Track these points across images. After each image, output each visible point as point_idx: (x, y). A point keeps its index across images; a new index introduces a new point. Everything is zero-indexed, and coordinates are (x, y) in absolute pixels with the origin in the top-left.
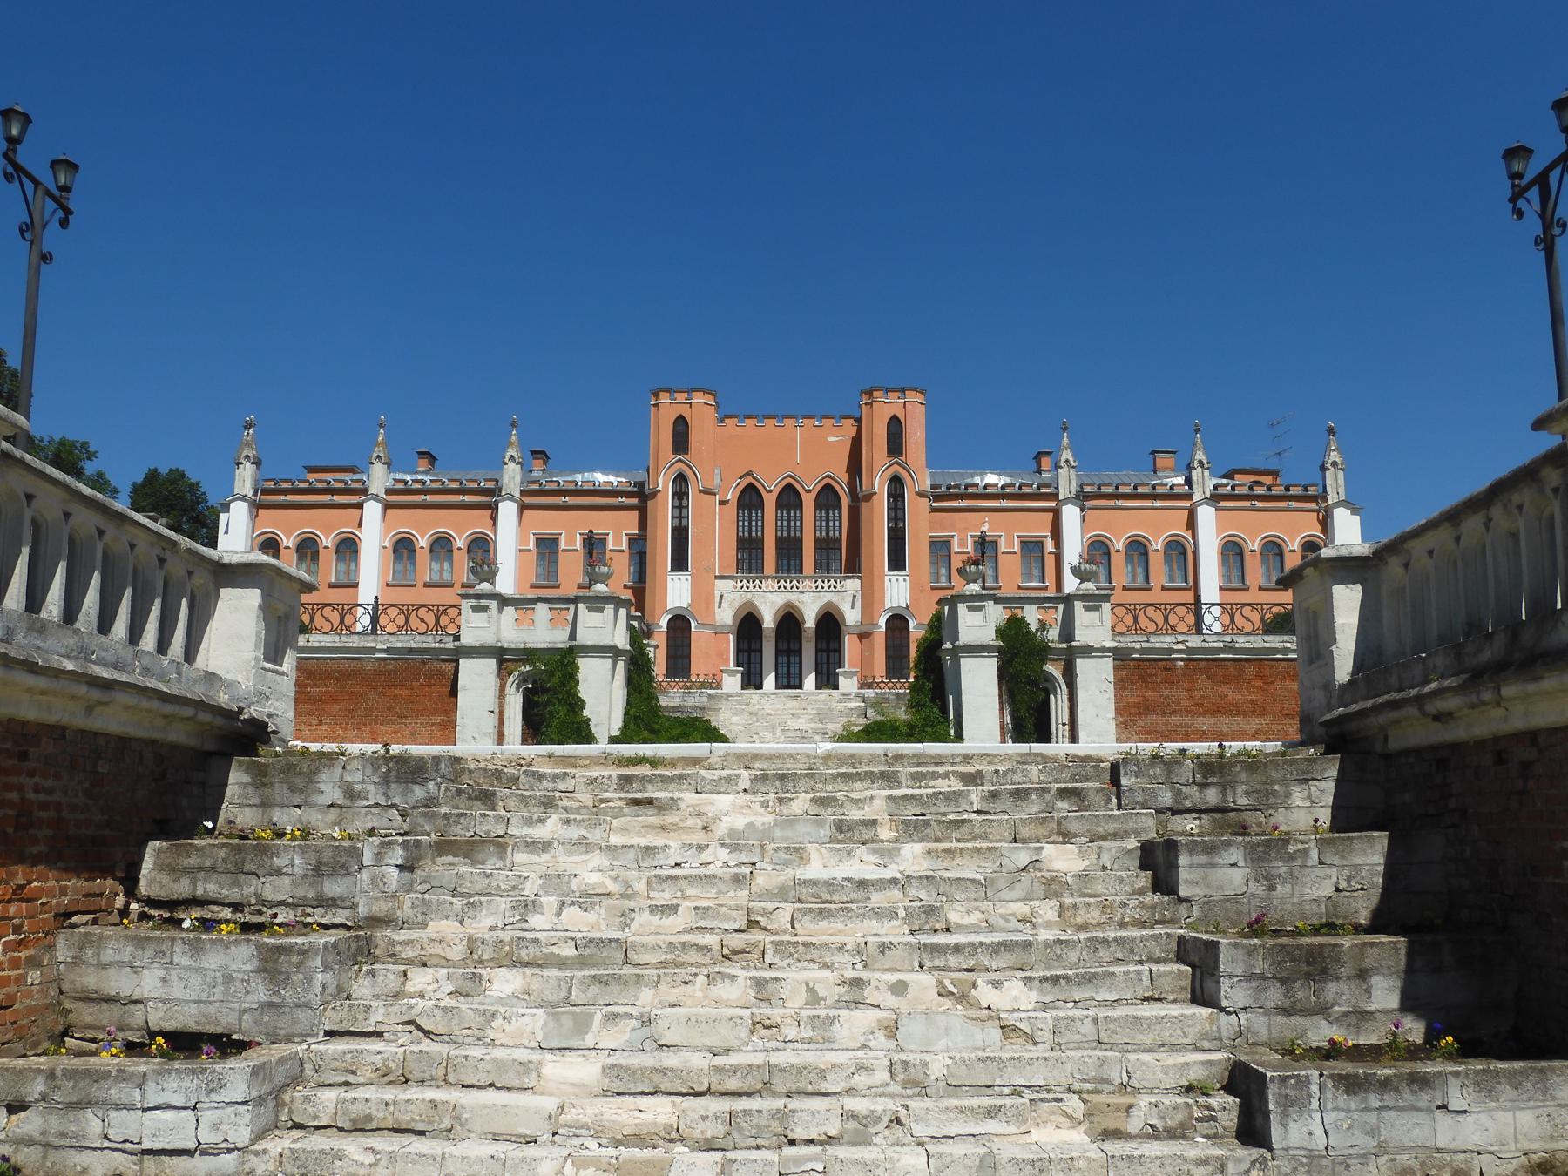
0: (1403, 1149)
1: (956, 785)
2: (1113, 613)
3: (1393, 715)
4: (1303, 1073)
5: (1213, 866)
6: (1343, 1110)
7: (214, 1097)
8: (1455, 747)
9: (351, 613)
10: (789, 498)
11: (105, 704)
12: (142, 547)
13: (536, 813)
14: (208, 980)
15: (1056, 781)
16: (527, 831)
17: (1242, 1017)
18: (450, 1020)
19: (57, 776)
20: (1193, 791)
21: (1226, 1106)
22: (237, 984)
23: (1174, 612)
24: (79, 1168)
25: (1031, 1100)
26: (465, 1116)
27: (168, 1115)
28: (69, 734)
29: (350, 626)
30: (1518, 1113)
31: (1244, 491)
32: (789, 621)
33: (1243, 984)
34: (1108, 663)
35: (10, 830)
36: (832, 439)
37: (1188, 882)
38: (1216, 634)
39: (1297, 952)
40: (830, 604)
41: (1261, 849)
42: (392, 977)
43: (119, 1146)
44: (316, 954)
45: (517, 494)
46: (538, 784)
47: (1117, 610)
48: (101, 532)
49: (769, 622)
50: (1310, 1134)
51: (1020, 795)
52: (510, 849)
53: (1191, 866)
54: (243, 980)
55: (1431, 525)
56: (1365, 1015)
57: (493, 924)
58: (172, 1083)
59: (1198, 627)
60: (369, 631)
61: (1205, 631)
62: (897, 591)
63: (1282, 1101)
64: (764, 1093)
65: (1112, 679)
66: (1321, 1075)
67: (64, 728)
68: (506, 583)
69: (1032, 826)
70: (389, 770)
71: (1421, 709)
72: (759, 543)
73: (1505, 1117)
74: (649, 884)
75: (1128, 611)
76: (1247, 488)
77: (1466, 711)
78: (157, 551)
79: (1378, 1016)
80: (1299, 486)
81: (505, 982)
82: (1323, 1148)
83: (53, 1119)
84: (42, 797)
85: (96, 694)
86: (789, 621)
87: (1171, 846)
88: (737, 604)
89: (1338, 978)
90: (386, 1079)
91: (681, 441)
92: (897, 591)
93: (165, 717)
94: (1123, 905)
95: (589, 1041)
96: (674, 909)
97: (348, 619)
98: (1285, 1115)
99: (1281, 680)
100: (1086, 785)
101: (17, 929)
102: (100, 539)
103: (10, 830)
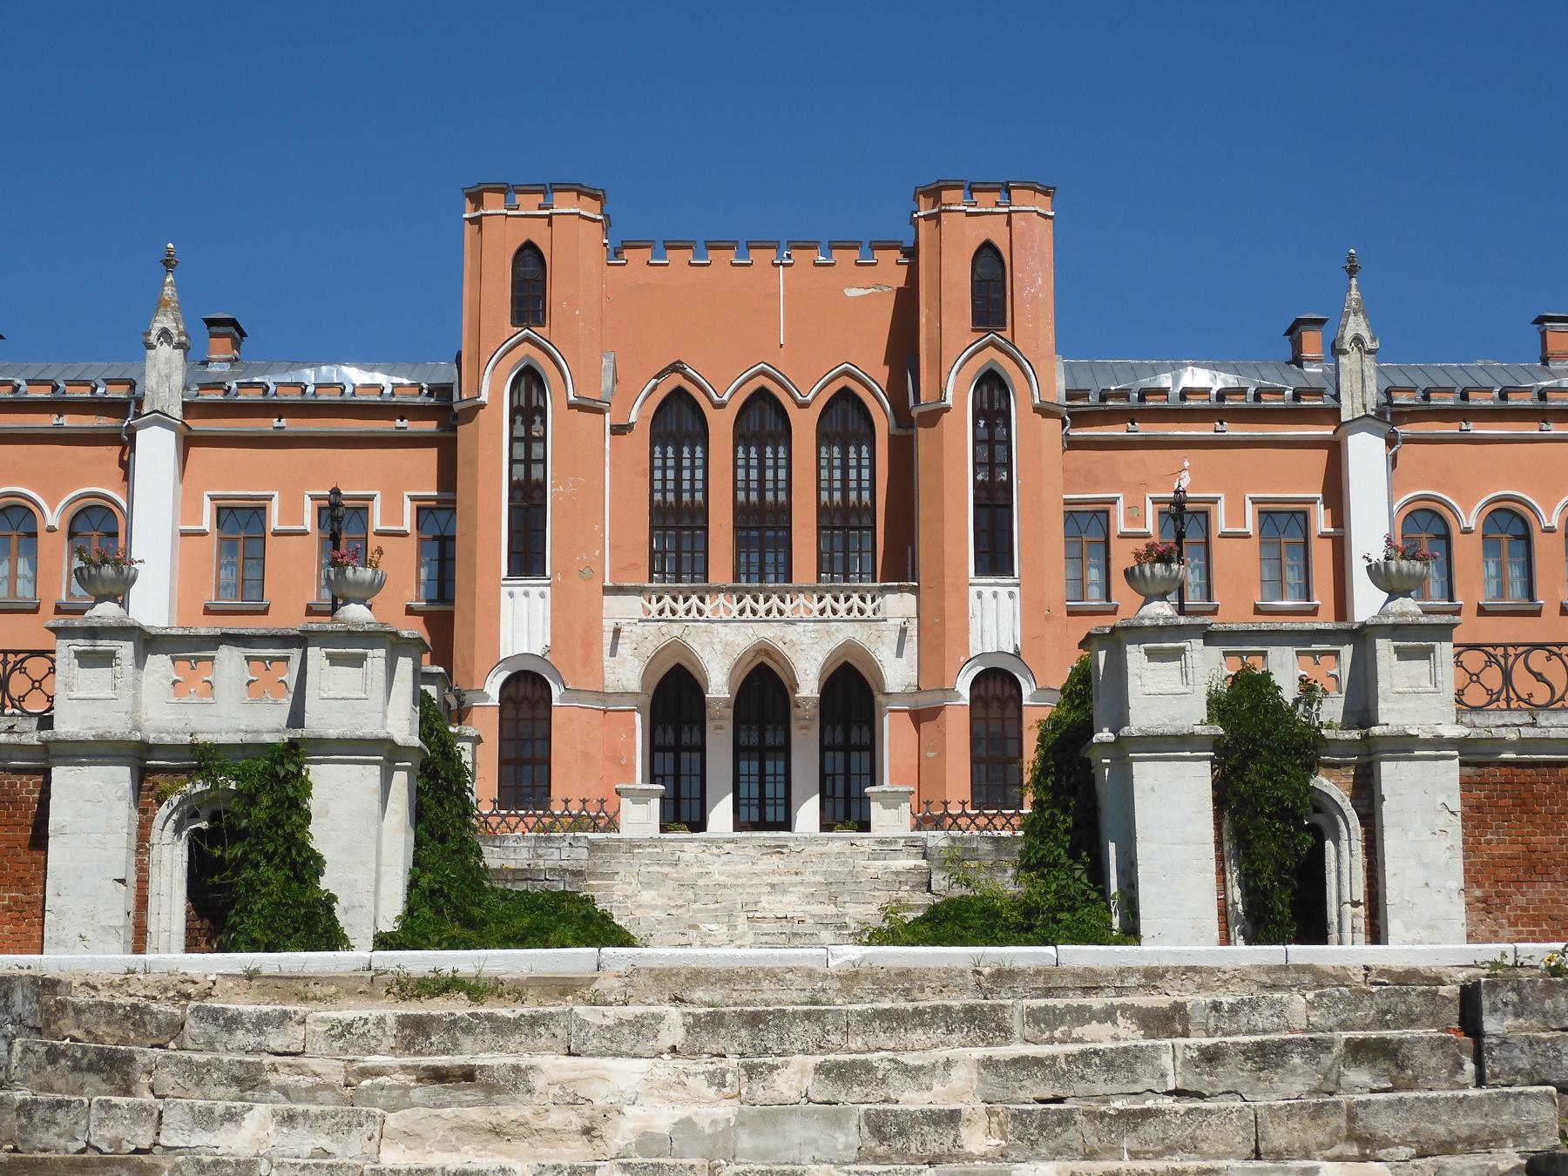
1: (1129, 1035)
2: (1459, 664)
13: (222, 1099)
15: (1343, 1026)
16: (200, 1139)
40: (850, 646)
49: (719, 685)
65: (1456, 805)
69: (1294, 1123)
75: (1491, 660)
88: (650, 649)
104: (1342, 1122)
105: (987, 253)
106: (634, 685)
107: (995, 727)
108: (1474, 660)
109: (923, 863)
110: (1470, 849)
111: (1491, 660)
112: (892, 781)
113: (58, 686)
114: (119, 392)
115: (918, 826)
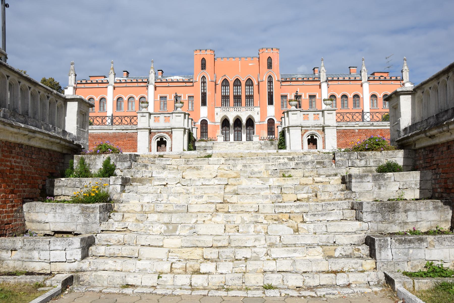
0: (415, 260)
1: (286, 160)
2: (336, 115)
3: (417, 137)
4: (386, 238)
5: (362, 182)
6: (397, 248)
7: (70, 247)
8: (435, 146)
9: (105, 119)
10: (237, 83)
11: (34, 137)
12: (42, 92)
13: (161, 170)
14: (67, 216)
15: (316, 159)
16: (158, 175)
17: (369, 224)
18: (137, 228)
19: (21, 159)
20: (358, 161)
21: (365, 250)
22: (75, 217)
23: (355, 115)
24: (33, 267)
25: (306, 248)
26: (142, 253)
27: (58, 252)
28: (24, 147)
29: (105, 123)
30: (450, 249)
31: (377, 78)
32: (238, 122)
33: (370, 214)
34: (335, 131)
35: (8, 173)
36: (250, 64)
37: (355, 187)
38: (368, 121)
39: (386, 205)
40: (250, 115)
41: (377, 177)
42: (120, 216)
43: (44, 261)
44: (97, 208)
45: (154, 83)
46: (161, 162)
47: (338, 114)
48: (30, 88)
50: (388, 255)
51: (306, 163)
52: (153, 181)
53: (356, 182)
54: (77, 216)
55: (431, 80)
56: (406, 223)
57: (148, 201)
58: (58, 243)
59: (363, 119)
60: (110, 125)
61: (365, 121)
62: (271, 111)
63: (380, 246)
64: (229, 247)
65: (336, 135)
66: (391, 239)
67: (22, 145)
68: (151, 109)
69: (309, 172)
70: (117, 158)
71: (425, 134)
72: (228, 97)
73: (446, 251)
74: (194, 190)
75: (341, 115)
76: (378, 78)
77: (439, 134)
78: (46, 94)
79: (410, 223)
81: (153, 217)
82: (391, 259)
83: (24, 254)
84: (17, 164)
85: (31, 134)
86: (238, 122)
87: (350, 176)
89: (398, 213)
90: (119, 244)
91: (203, 66)
92: (271, 111)
93: (51, 142)
94: (335, 194)
95: (177, 233)
96: (202, 197)
97: (104, 121)
98: (380, 250)
99: (388, 135)
100: (325, 160)
101: (12, 202)
102: (30, 90)
103: (8, 173)
104: (316, 172)
105: (269, 58)
106: (220, 121)
107: (271, 127)
108: (339, 115)
109: (261, 145)
110: (338, 142)
111: (341, 115)
112: (256, 134)
113: (138, 121)
114: (146, 81)
115: (260, 140)
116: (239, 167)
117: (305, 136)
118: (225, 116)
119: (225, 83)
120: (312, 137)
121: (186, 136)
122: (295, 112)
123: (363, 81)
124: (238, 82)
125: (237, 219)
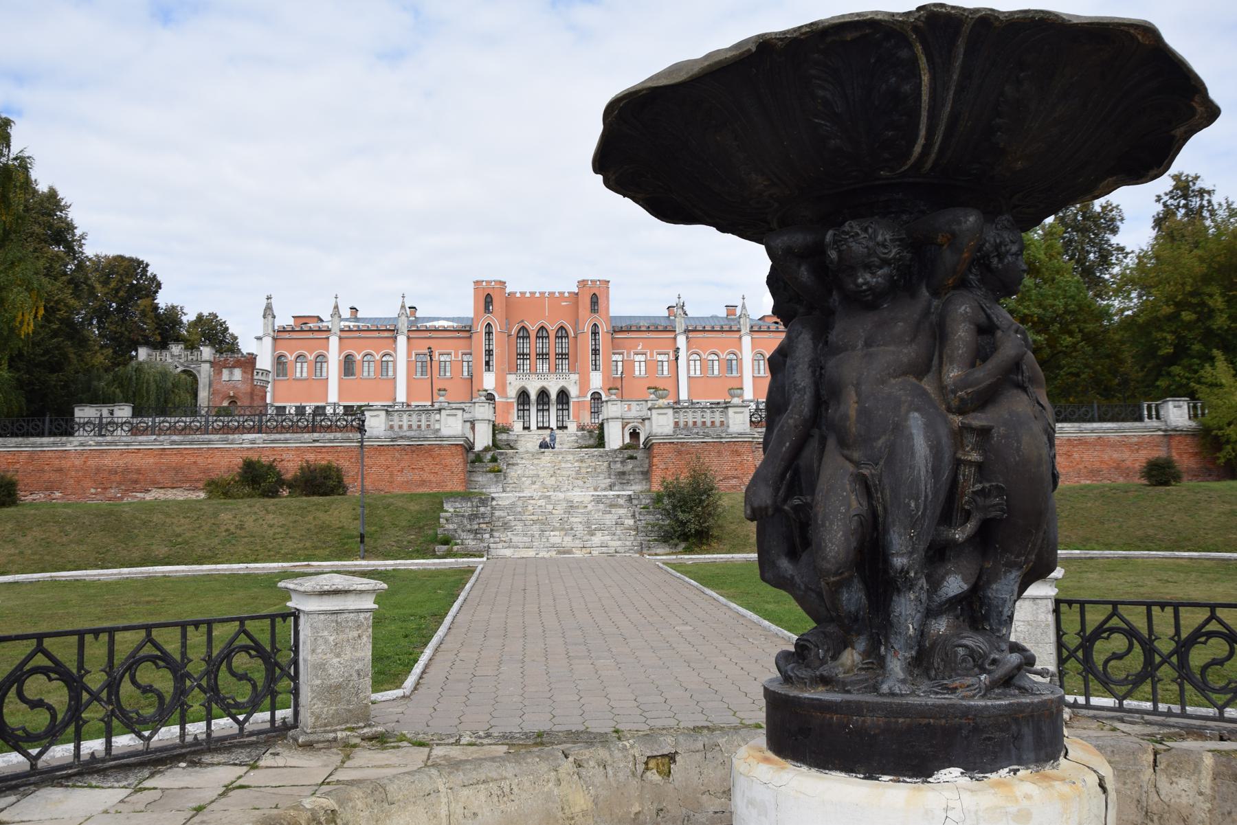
32: (543, 394)
45: (406, 332)
80: (233, 620)
86: (543, 394)
88: (518, 388)
106: (514, 396)
116: (560, 458)
117: (626, 429)
118: (523, 387)
119: (523, 333)
120: (634, 430)
121: (491, 426)
122: (615, 402)
123: (742, 332)
124: (544, 332)
125: (560, 479)
